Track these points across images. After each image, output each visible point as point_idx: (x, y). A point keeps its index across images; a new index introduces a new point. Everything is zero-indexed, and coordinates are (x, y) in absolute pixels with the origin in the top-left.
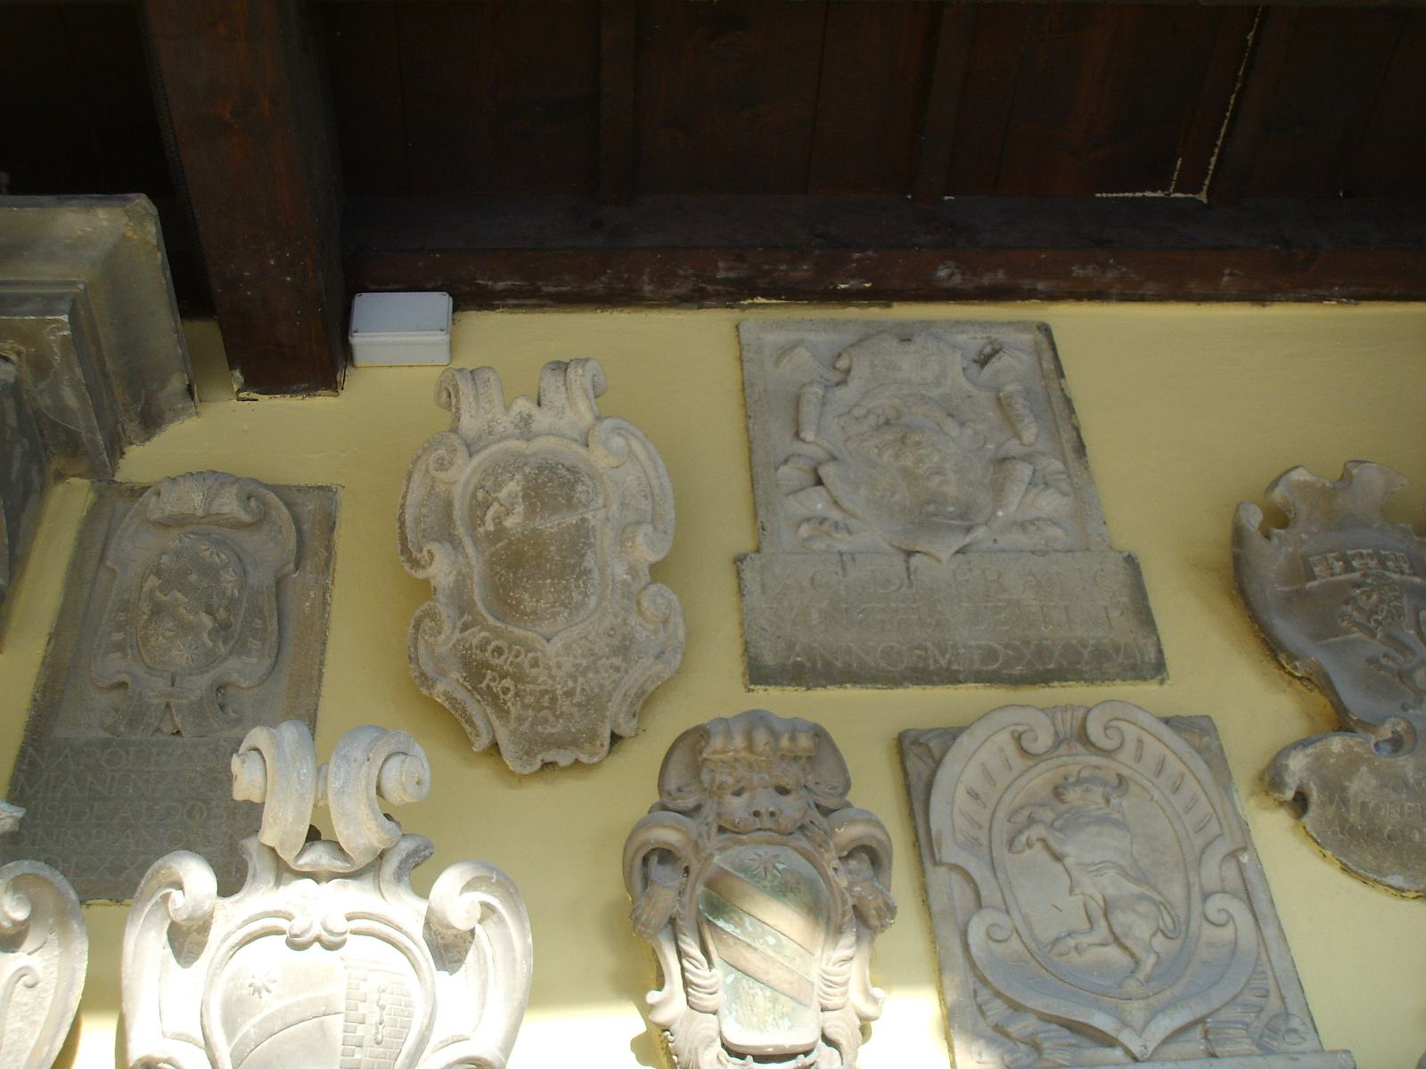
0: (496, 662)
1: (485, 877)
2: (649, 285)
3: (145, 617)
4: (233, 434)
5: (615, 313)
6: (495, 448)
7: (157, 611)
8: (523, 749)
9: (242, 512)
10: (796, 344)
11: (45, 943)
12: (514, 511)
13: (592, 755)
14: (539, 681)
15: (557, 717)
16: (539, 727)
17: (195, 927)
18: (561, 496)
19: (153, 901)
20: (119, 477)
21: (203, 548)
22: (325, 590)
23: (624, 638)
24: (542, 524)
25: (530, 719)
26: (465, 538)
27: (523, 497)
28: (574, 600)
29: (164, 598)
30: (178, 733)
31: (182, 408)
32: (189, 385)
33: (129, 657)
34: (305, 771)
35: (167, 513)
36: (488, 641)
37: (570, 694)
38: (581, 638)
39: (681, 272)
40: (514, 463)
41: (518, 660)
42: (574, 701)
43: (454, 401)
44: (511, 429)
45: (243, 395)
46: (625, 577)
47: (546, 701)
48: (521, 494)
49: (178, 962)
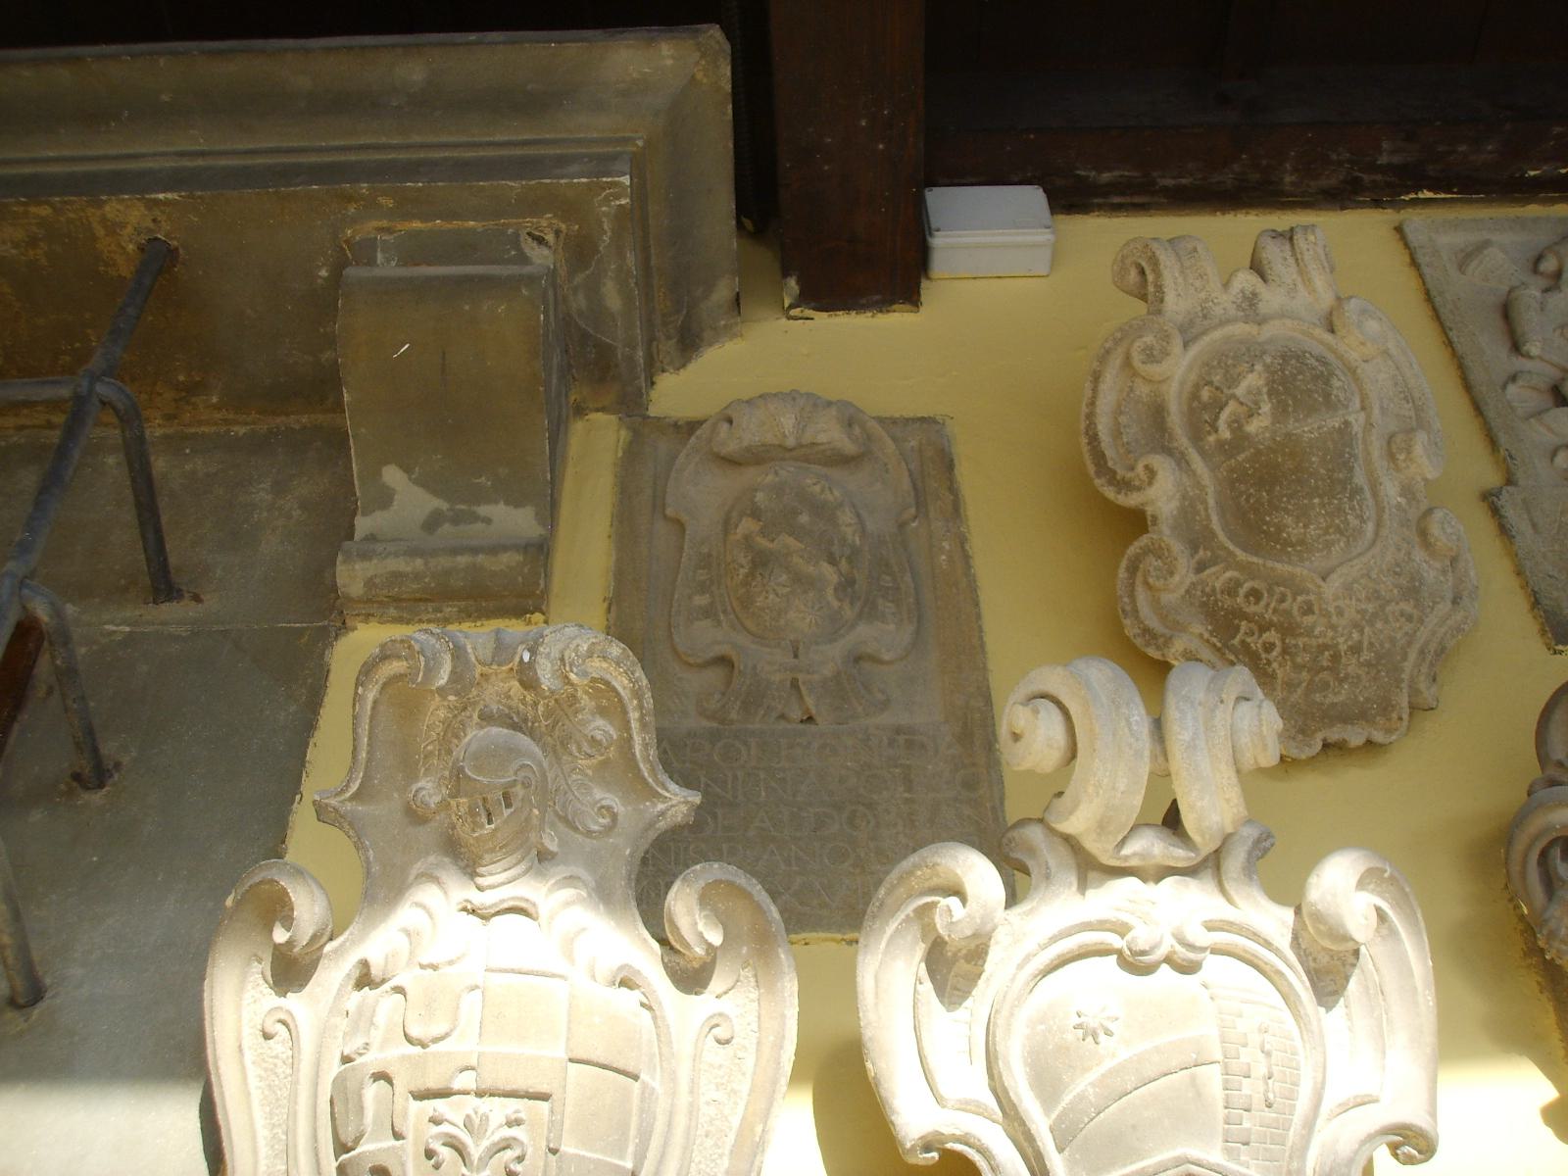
0: (1252, 609)
1: (1377, 868)
2: (1291, 175)
3: (743, 571)
4: (780, 361)
5: (1239, 216)
6: (1217, 334)
7: (761, 562)
8: (1295, 727)
9: (846, 440)
10: (1486, 244)
11: (738, 981)
12: (1260, 411)
13: (1389, 731)
14: (1316, 632)
15: (1341, 681)
16: (1318, 695)
17: (964, 952)
18: (1317, 392)
19: (901, 916)
20: (653, 412)
21: (809, 481)
22: (962, 541)
23: (1413, 579)
24: (1298, 428)
25: (1304, 685)
26: (1190, 450)
27: (1270, 394)
28: (1351, 526)
29: (771, 546)
30: (810, 719)
31: (725, 326)
32: (738, 294)
33: (724, 624)
34: (1136, 718)
35: (745, 444)
36: (1238, 584)
37: (1356, 649)
38: (1362, 576)
39: (1334, 157)
40: (1249, 353)
41: (1285, 605)
42: (1361, 660)
43: (1150, 277)
44: (1232, 312)
45: (794, 312)
46: (1399, 499)
47: (1325, 660)
48: (1265, 390)
49: (942, 1002)
